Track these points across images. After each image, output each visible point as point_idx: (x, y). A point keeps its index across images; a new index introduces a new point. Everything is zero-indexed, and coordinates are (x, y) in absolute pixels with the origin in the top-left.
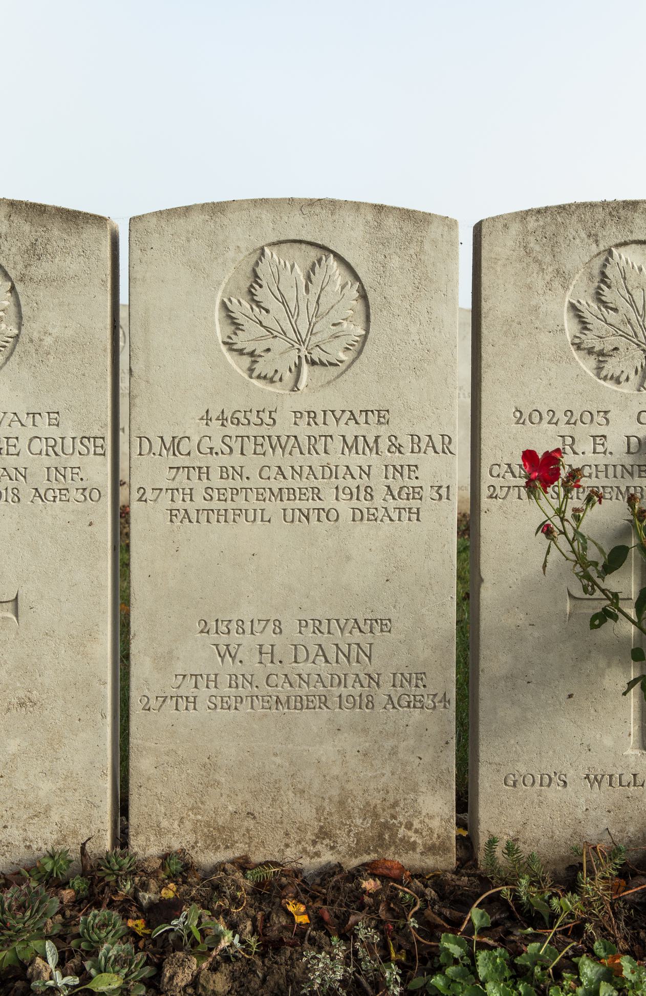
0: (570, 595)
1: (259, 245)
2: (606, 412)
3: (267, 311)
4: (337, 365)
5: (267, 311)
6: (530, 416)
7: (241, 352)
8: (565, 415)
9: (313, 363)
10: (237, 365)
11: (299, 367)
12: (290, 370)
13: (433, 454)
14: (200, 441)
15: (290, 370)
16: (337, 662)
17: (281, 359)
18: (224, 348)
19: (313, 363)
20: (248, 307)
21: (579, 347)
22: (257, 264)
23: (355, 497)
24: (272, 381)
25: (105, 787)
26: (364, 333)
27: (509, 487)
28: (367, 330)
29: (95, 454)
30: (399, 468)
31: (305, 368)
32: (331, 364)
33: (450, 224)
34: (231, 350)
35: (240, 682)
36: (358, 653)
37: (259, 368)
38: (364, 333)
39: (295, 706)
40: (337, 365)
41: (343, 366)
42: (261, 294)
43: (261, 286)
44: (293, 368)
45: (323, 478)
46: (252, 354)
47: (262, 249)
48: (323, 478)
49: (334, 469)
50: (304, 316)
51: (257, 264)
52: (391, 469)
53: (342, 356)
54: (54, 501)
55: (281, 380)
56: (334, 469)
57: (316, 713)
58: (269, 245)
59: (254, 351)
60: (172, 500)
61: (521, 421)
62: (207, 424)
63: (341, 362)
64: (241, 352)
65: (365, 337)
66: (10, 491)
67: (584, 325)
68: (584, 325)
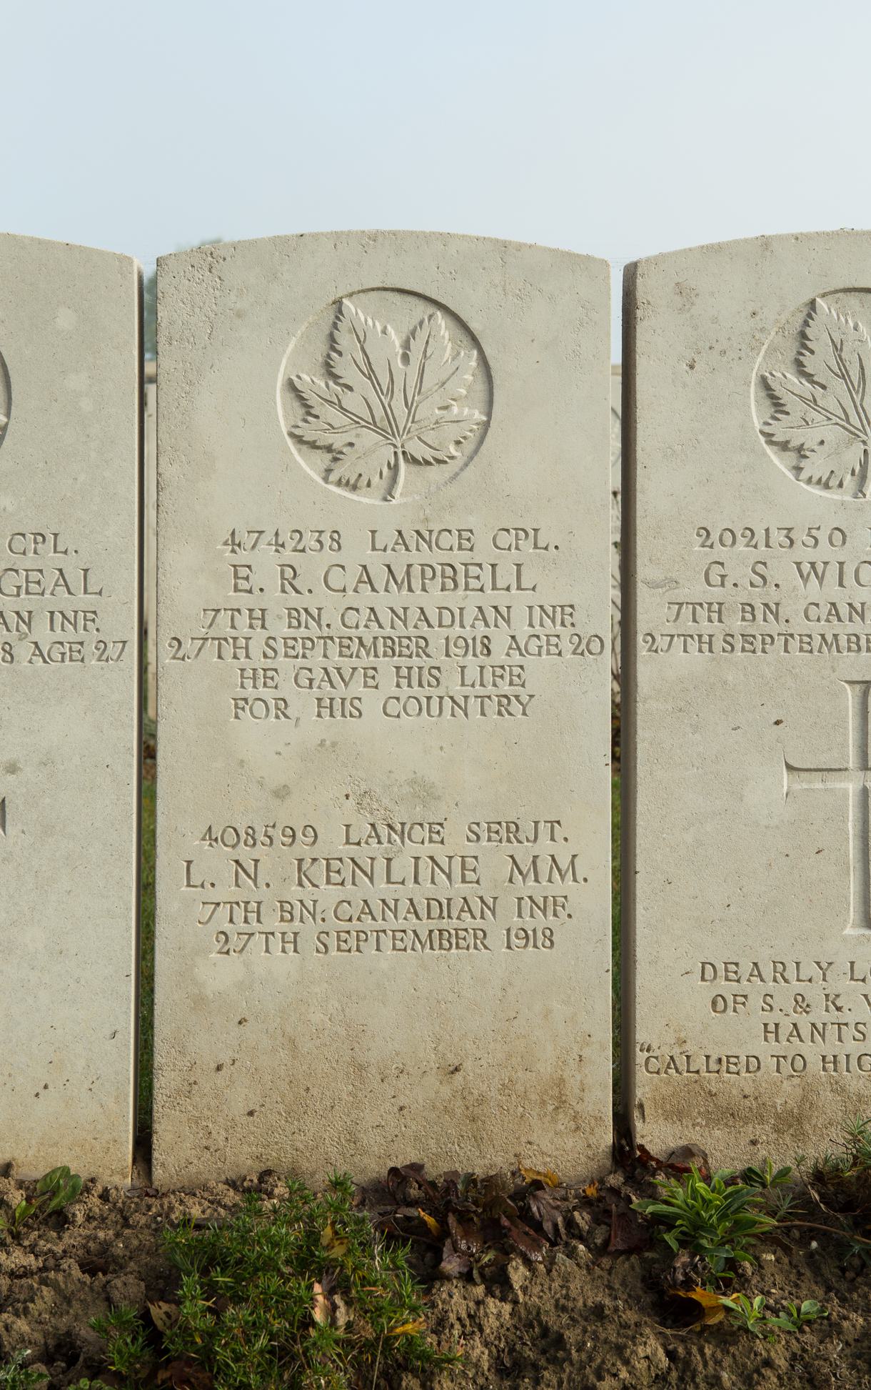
0: (790, 768)
1: (806, 298)
2: (789, 530)
3: (824, 387)
4: (445, 462)
5: (350, 388)
6: (721, 536)
7: (313, 445)
8: (698, 535)
9: (415, 461)
10: (309, 466)
11: (394, 469)
12: (853, 471)
13: (67, 595)
14: (709, 569)
15: (853, 473)
16: (433, 882)
17: (372, 453)
18: (289, 441)
19: (415, 461)
20: (323, 385)
21: (299, 440)
22: (806, 324)
23: (471, 652)
24: (355, 488)
25: (605, 1034)
26: (485, 418)
27: (672, 636)
28: (489, 415)
29: (467, 588)
30: (401, 612)
31: (402, 465)
32: (439, 461)
33: (605, 264)
34: (770, 443)
35: (297, 913)
36: (354, 872)
37: (809, 468)
38: (485, 418)
39: (441, 944)
40: (445, 462)
41: (453, 467)
42: (344, 367)
43: (340, 354)
44: (385, 470)
45: (440, 625)
46: (800, 449)
47: (813, 302)
48: (440, 625)
49: (457, 612)
50: (399, 395)
51: (806, 324)
52: (58, 617)
53: (453, 450)
54: (540, 654)
55: (369, 485)
56: (457, 612)
57: (471, 955)
58: (823, 296)
59: (788, 442)
60: (325, 656)
61: (753, 543)
62: (277, 551)
63: (452, 458)
64: (313, 445)
65: (487, 425)
66: (478, 641)
67: (777, 404)
68: (777, 404)
